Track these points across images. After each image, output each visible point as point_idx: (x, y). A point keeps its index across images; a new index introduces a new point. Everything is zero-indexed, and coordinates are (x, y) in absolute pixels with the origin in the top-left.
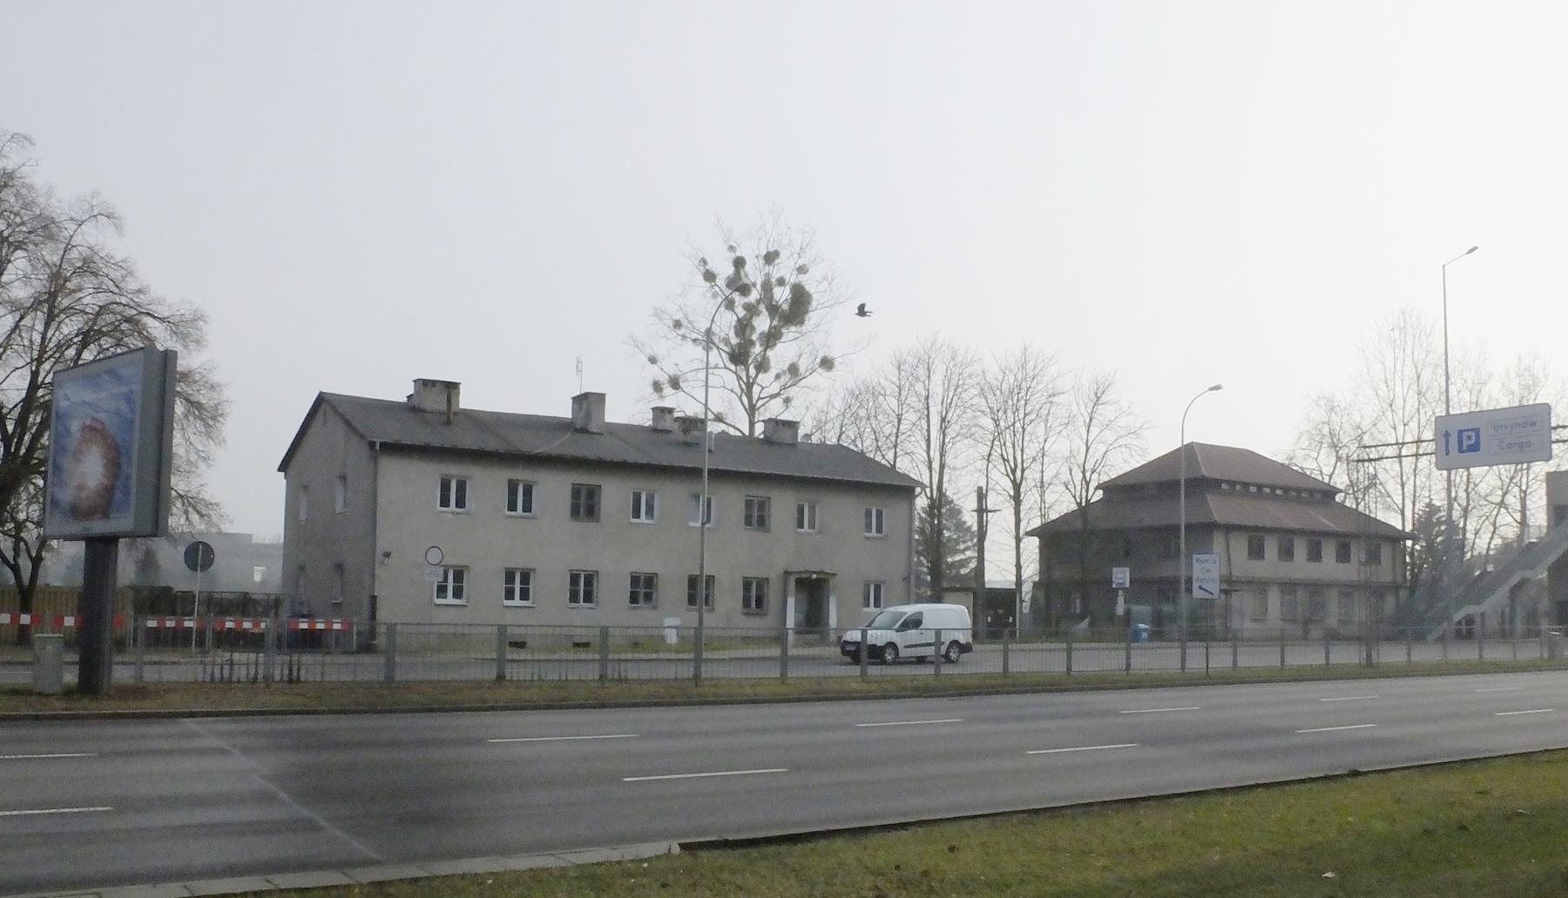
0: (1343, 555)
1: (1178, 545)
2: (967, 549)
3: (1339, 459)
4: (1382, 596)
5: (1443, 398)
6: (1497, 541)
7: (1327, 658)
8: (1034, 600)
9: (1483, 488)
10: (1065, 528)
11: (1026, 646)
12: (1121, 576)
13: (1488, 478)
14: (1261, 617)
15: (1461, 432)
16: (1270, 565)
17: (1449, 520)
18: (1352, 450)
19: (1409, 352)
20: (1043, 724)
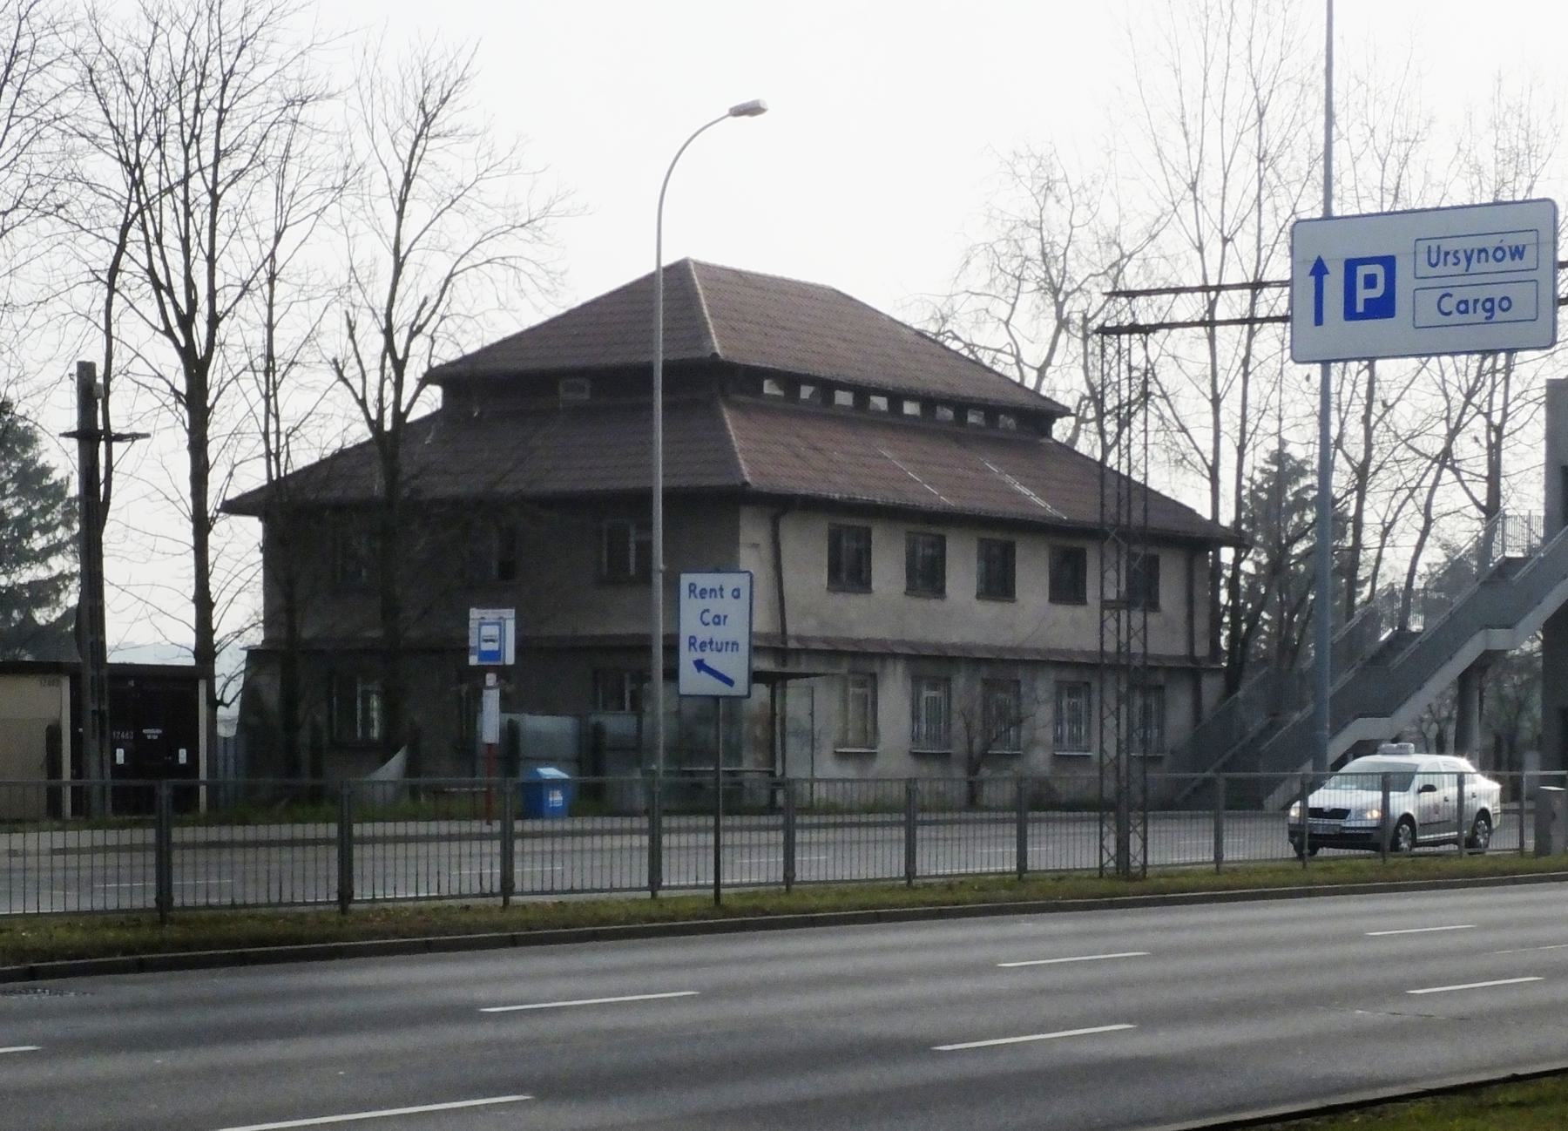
0: (1067, 586)
1: (645, 549)
2: (56, 548)
3: (1063, 324)
4: (872, 681)
5: (1319, 172)
6: (1433, 556)
7: (1022, 856)
8: (250, 695)
9: (1404, 417)
10: (335, 493)
11: (225, 833)
12: (493, 631)
13: (1416, 389)
14: (860, 747)
15: (1351, 266)
16: (885, 608)
17: (1325, 500)
18: (1089, 303)
19: (1240, 43)
20: (271, 1051)
